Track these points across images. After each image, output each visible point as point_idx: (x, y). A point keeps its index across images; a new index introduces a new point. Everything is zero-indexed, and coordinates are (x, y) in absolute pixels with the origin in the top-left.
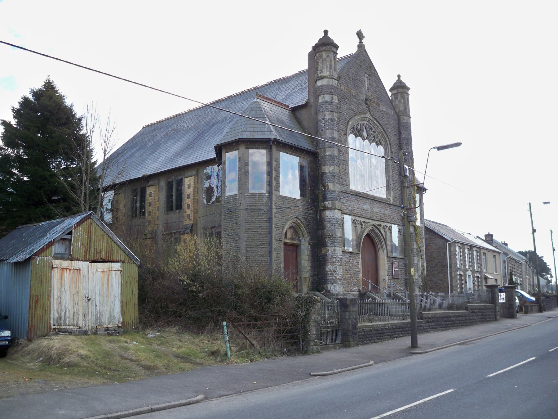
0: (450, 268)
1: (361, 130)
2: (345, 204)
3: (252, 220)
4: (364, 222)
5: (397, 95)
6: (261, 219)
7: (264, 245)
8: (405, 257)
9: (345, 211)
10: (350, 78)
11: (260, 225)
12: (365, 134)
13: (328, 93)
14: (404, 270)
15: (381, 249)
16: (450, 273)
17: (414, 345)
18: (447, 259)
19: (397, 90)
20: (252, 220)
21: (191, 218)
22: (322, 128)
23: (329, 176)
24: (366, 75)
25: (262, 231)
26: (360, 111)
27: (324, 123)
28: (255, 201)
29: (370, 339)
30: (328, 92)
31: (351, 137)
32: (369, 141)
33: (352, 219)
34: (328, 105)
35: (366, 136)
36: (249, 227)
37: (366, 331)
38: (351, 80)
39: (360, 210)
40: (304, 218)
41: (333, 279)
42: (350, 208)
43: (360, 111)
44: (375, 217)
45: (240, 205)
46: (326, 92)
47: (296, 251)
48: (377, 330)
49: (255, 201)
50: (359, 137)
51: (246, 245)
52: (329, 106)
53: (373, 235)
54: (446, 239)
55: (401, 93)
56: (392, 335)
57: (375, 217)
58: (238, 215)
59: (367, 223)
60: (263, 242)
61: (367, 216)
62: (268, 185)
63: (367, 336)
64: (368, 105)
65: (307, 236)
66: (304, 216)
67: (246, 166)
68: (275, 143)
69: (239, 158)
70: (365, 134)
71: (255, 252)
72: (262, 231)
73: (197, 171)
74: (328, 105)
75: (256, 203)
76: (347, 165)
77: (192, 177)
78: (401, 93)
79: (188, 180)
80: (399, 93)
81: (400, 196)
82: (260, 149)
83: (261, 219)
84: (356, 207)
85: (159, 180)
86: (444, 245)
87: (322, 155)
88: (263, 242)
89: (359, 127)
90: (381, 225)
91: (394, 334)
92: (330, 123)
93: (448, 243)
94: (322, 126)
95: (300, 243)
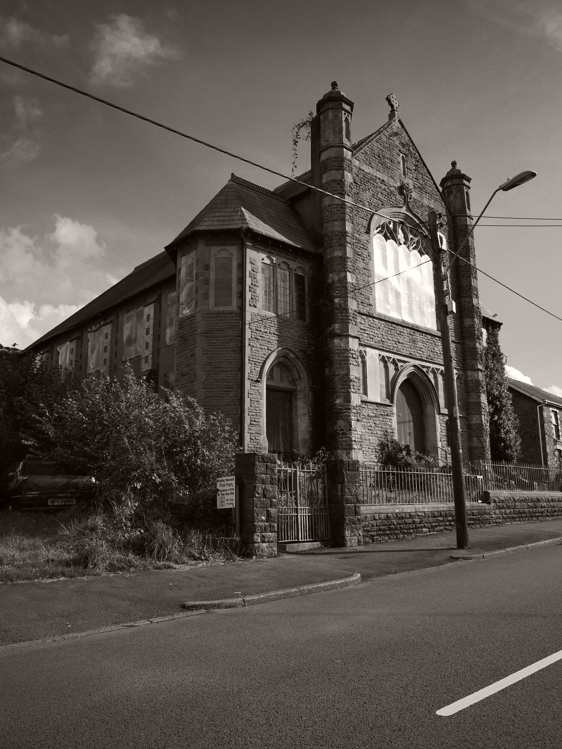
0: (542, 440)
1: (395, 230)
2: (368, 332)
3: (214, 350)
4: (400, 361)
5: (452, 188)
6: (227, 348)
7: (233, 388)
8: (468, 415)
9: (368, 342)
10: (374, 154)
11: (225, 357)
12: (401, 236)
13: (336, 168)
14: (467, 434)
15: (429, 402)
16: (543, 446)
17: (462, 543)
18: (538, 429)
19: (452, 182)
20: (214, 350)
21: (149, 361)
22: (329, 218)
23: (338, 287)
24: (401, 155)
25: (228, 366)
26: (392, 203)
27: (331, 212)
28: (218, 322)
29: (388, 532)
30: (336, 166)
31: (377, 240)
32: (408, 247)
33: (380, 355)
34: (335, 185)
35: (402, 240)
36: (209, 361)
37: (379, 519)
38: (377, 158)
39: (393, 343)
40: (301, 351)
41: (345, 441)
42: (376, 338)
43: (392, 203)
44: (418, 355)
45: (196, 329)
46: (333, 166)
47: (291, 400)
48: (402, 518)
49: (218, 322)
50: (392, 240)
51: (204, 388)
52: (338, 186)
53: (416, 381)
54: (536, 401)
55: (456, 185)
56: (432, 527)
57: (418, 355)
58: (194, 344)
59: (405, 362)
60: (231, 384)
61: (405, 352)
62: (239, 297)
63: (382, 527)
64: (404, 195)
65: (304, 375)
66: (300, 348)
67: (206, 271)
68: (249, 235)
69: (197, 261)
70: (401, 236)
71: (218, 399)
72: (228, 366)
73: (160, 296)
74: (335, 185)
75: (221, 324)
76: (371, 277)
77: (152, 305)
78: (456, 185)
79: (148, 309)
80: (453, 185)
81: (459, 328)
82: (227, 245)
83: (227, 348)
84: (386, 337)
85: (117, 317)
86: (533, 409)
87: (329, 257)
88: (231, 384)
89: (391, 226)
90: (428, 367)
91: (436, 526)
92: (340, 211)
93: (538, 406)
94: (328, 216)
95: (295, 388)
